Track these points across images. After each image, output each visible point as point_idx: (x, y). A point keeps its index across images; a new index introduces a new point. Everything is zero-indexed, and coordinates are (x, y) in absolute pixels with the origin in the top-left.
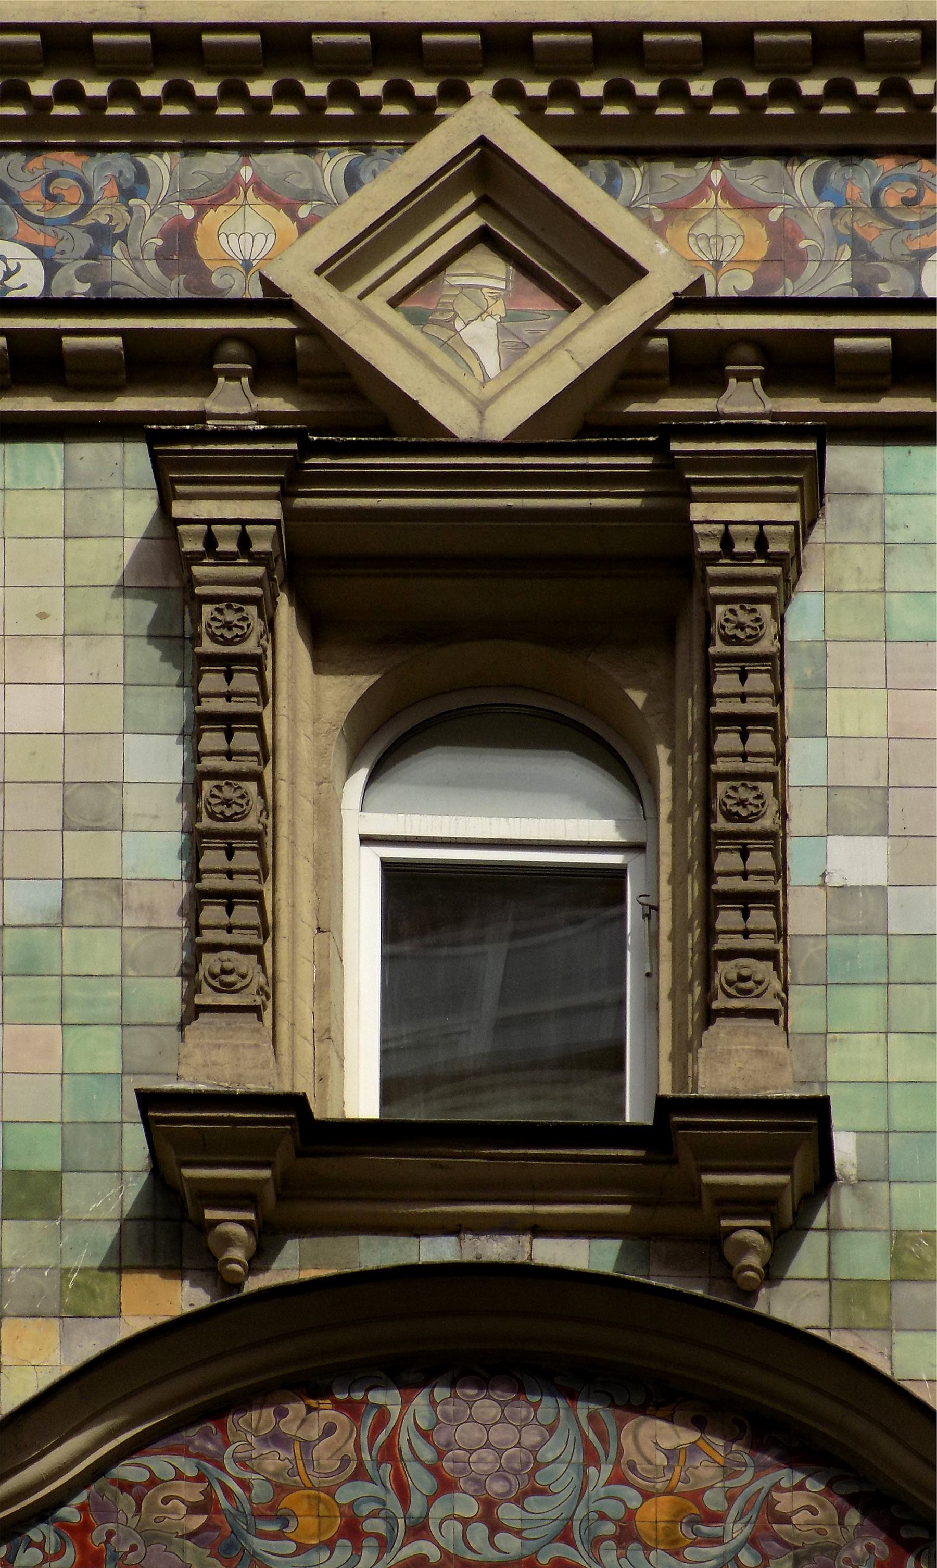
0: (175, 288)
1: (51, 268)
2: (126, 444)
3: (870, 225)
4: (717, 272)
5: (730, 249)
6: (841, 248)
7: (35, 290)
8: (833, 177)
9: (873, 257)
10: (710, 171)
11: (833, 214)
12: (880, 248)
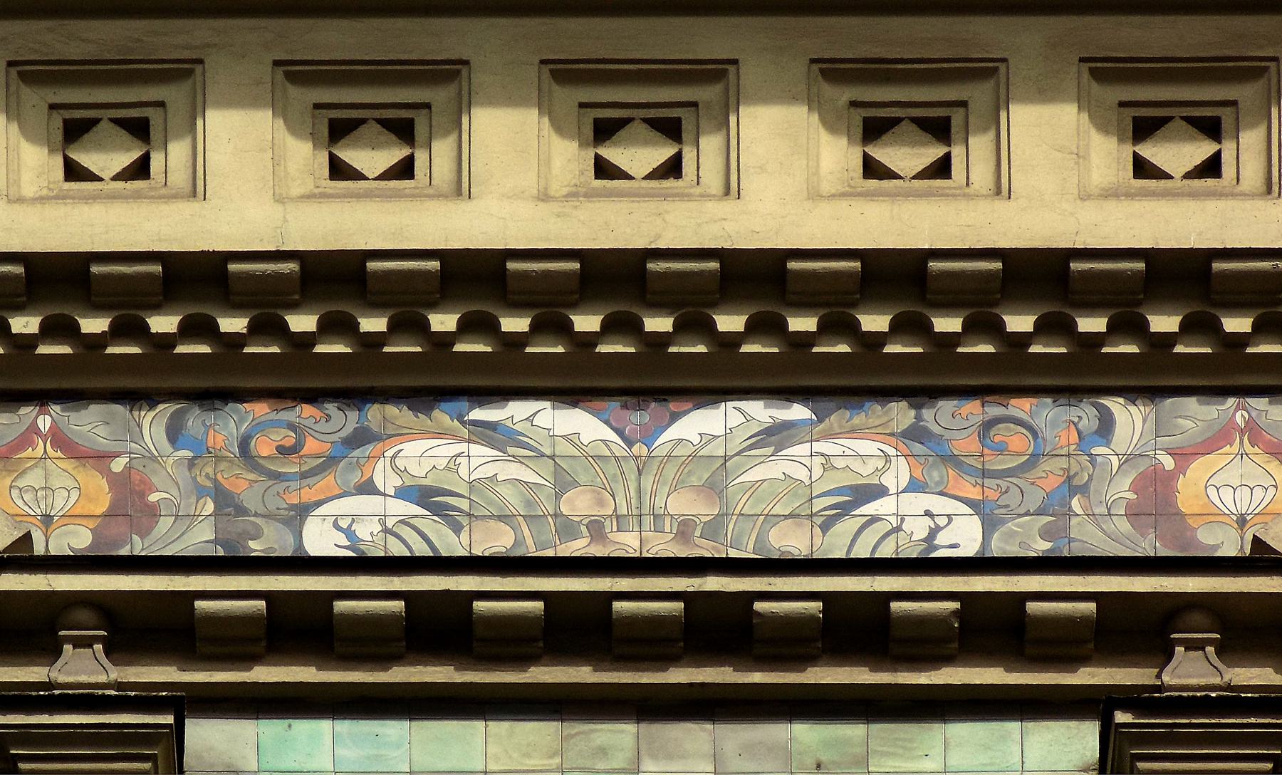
0: (1149, 546)
1: (990, 525)
2: (490, 723)
3: (237, 476)
4: (47, 527)
5: (60, 504)
6: (202, 501)
7: (969, 549)
8: (190, 423)
9: (241, 511)
10: (37, 417)
11: (191, 463)
12: (250, 500)
